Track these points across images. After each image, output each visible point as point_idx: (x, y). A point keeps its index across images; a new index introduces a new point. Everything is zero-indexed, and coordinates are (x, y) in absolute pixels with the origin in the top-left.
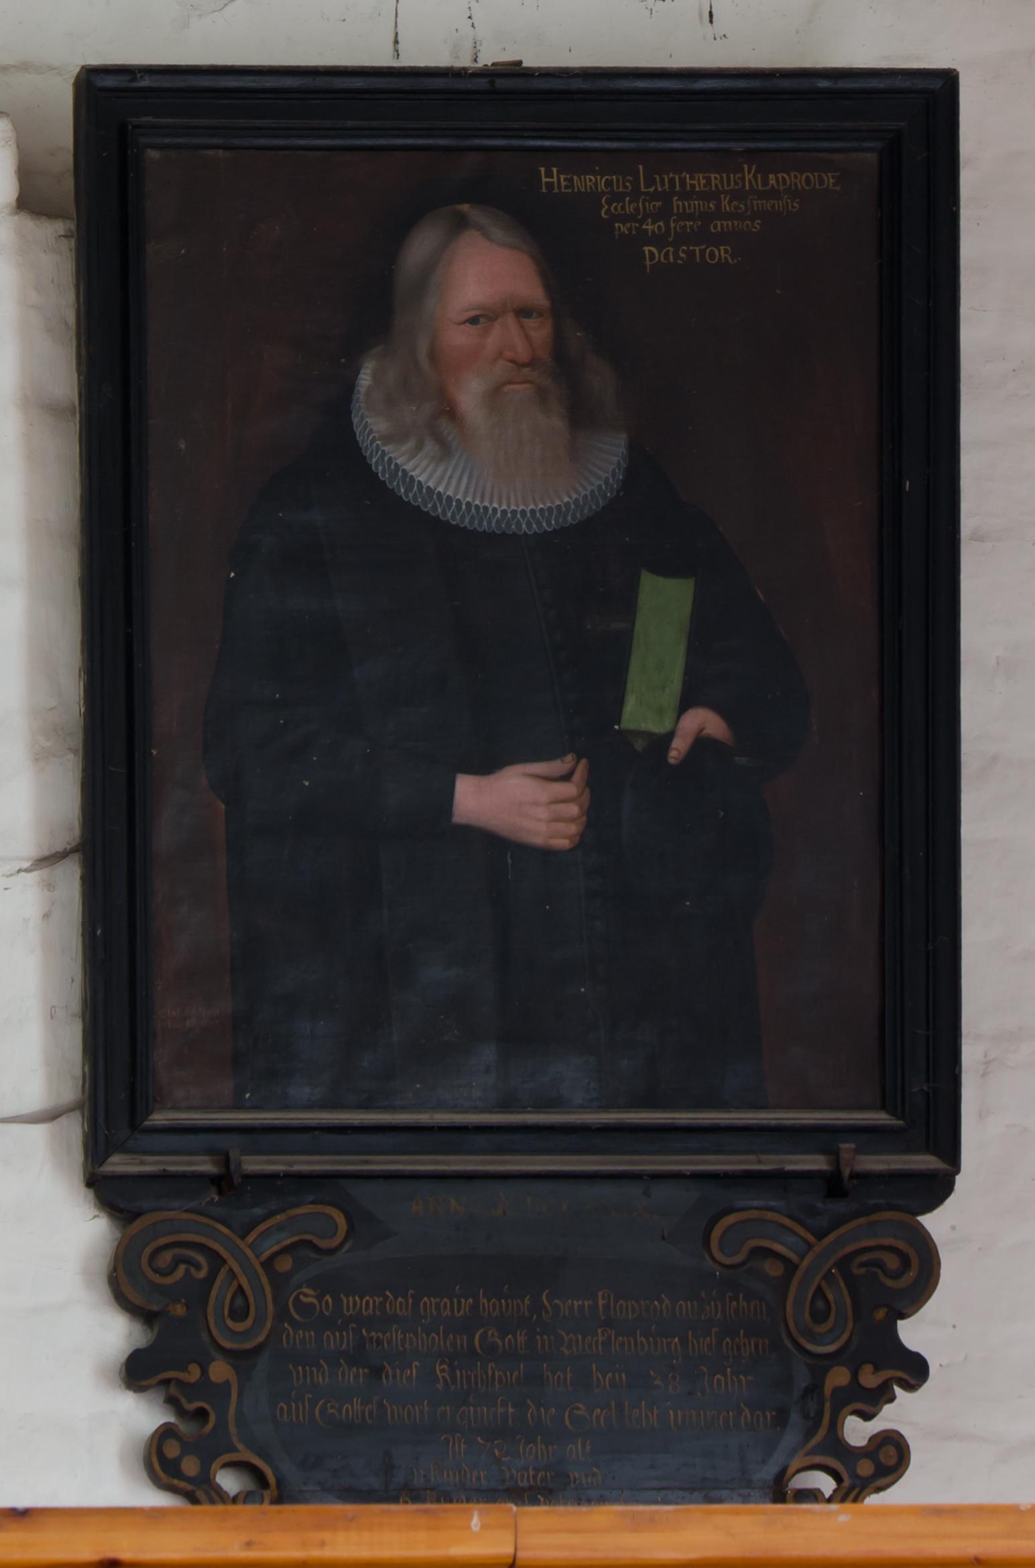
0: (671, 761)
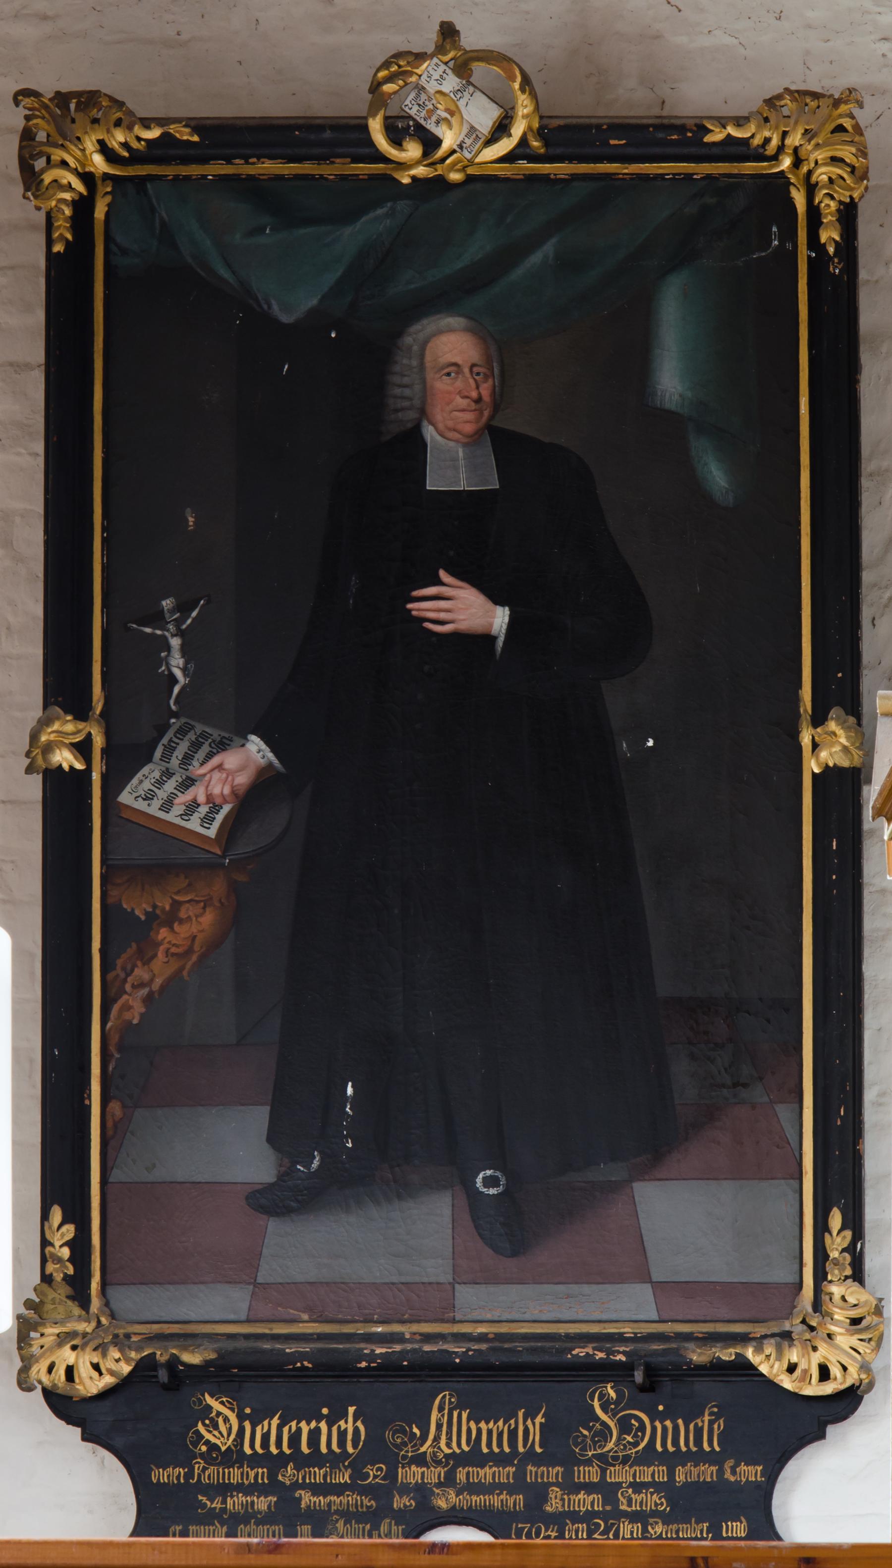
0: (499, 619)
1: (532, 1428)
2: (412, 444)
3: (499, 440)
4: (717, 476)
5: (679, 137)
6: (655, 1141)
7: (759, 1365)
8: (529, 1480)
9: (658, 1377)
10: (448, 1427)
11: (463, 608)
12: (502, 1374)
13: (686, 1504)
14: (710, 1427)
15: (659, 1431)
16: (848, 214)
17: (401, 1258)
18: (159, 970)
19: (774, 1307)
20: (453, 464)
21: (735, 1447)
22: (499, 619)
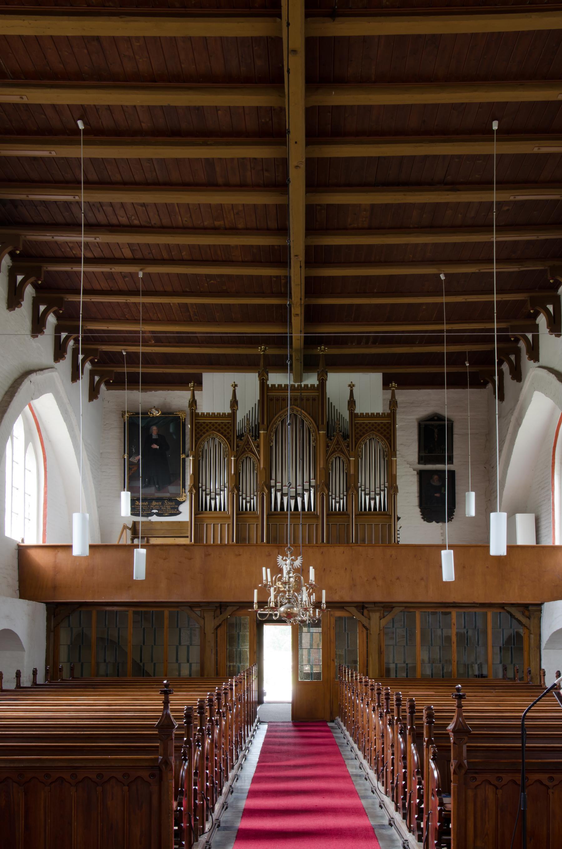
0: (158, 447)
1: (160, 503)
2: (151, 435)
3: (158, 435)
4: (175, 437)
5: (172, 413)
6: (170, 483)
7: (554, 543)
8: (269, 570)
9: (170, 500)
10: (154, 503)
11: (155, 446)
12: (158, 499)
13: (172, 508)
14: (174, 503)
15: (170, 503)
16: (185, 419)
17: (152, 491)
18: (132, 472)
19: (179, 495)
20: (155, 436)
21: (176, 504)
22: (158, 447)
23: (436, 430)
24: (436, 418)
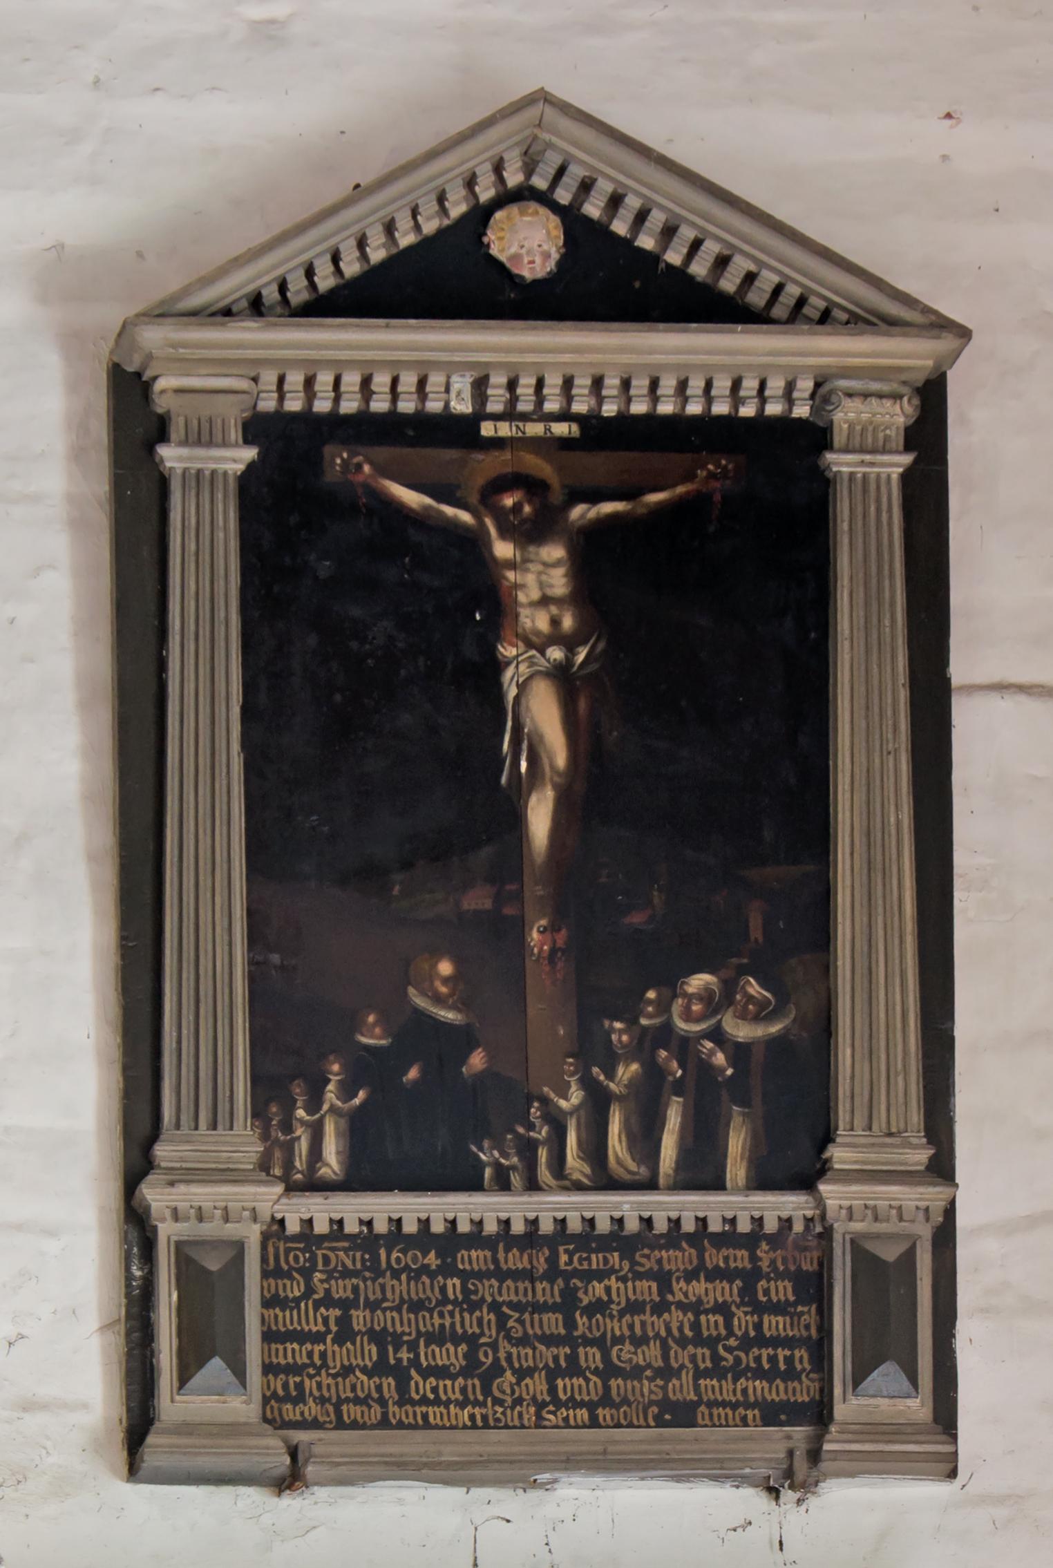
23: (538, 580)
24: (528, 244)
